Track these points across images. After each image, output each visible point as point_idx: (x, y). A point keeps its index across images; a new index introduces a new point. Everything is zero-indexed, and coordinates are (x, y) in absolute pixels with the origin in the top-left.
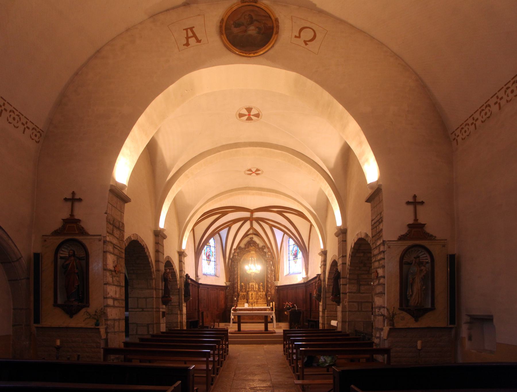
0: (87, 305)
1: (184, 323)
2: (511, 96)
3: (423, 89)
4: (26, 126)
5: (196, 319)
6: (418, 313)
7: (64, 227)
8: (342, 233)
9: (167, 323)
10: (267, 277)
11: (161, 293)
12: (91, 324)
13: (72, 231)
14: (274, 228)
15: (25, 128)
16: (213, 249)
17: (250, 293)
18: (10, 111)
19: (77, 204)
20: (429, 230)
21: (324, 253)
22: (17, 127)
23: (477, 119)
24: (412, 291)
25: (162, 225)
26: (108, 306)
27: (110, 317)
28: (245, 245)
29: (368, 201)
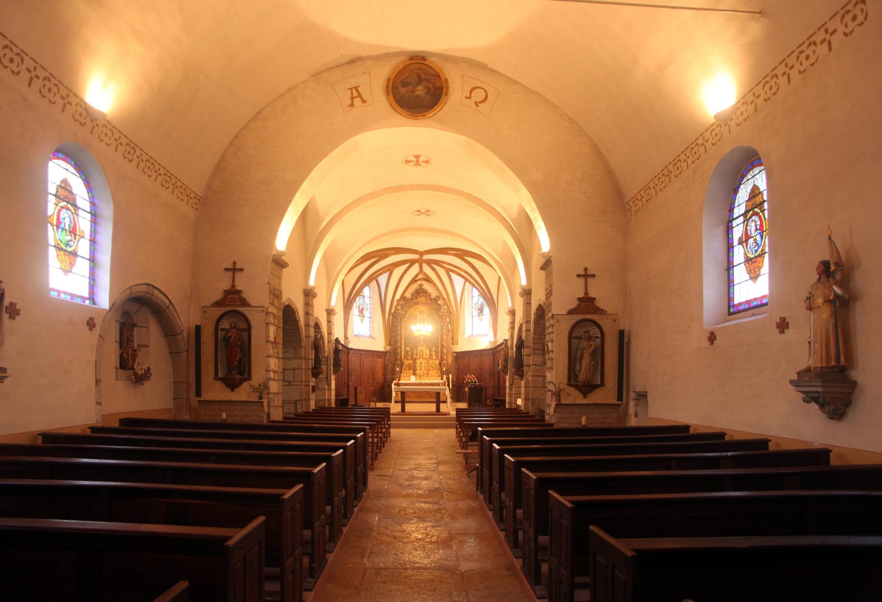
0: (249, 378)
1: (333, 402)
2: (806, 64)
3: (599, 154)
4: (33, 74)
5: (346, 397)
6: (587, 388)
7: (225, 297)
8: (527, 293)
9: (317, 402)
10: (442, 339)
11: (311, 363)
12: (254, 398)
13: (232, 302)
14: (451, 273)
15: (31, 78)
16: (367, 300)
17: (418, 362)
18: (45, 79)
19: (238, 274)
20: (599, 304)
21: (512, 313)
22: (54, 103)
23: (835, 31)
24: (581, 366)
25: (312, 283)
26: (270, 379)
27: (272, 391)
28: (412, 295)
29: (542, 269)
